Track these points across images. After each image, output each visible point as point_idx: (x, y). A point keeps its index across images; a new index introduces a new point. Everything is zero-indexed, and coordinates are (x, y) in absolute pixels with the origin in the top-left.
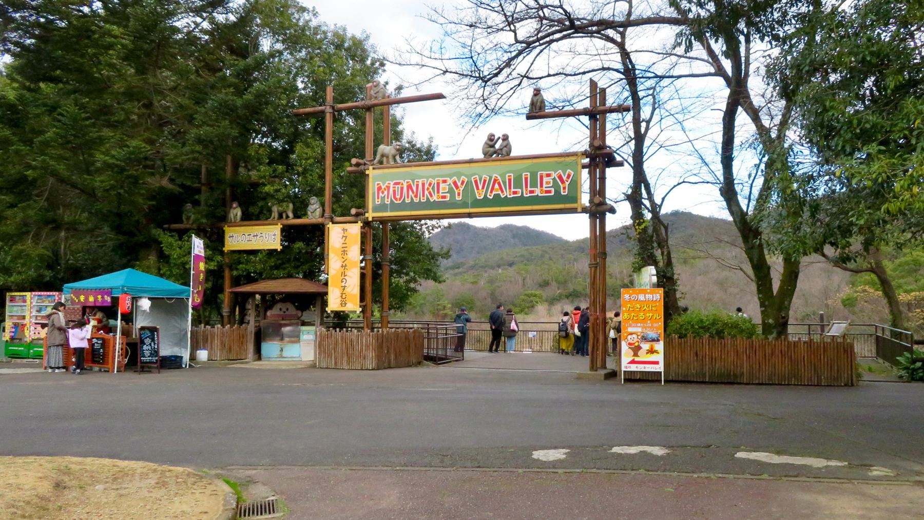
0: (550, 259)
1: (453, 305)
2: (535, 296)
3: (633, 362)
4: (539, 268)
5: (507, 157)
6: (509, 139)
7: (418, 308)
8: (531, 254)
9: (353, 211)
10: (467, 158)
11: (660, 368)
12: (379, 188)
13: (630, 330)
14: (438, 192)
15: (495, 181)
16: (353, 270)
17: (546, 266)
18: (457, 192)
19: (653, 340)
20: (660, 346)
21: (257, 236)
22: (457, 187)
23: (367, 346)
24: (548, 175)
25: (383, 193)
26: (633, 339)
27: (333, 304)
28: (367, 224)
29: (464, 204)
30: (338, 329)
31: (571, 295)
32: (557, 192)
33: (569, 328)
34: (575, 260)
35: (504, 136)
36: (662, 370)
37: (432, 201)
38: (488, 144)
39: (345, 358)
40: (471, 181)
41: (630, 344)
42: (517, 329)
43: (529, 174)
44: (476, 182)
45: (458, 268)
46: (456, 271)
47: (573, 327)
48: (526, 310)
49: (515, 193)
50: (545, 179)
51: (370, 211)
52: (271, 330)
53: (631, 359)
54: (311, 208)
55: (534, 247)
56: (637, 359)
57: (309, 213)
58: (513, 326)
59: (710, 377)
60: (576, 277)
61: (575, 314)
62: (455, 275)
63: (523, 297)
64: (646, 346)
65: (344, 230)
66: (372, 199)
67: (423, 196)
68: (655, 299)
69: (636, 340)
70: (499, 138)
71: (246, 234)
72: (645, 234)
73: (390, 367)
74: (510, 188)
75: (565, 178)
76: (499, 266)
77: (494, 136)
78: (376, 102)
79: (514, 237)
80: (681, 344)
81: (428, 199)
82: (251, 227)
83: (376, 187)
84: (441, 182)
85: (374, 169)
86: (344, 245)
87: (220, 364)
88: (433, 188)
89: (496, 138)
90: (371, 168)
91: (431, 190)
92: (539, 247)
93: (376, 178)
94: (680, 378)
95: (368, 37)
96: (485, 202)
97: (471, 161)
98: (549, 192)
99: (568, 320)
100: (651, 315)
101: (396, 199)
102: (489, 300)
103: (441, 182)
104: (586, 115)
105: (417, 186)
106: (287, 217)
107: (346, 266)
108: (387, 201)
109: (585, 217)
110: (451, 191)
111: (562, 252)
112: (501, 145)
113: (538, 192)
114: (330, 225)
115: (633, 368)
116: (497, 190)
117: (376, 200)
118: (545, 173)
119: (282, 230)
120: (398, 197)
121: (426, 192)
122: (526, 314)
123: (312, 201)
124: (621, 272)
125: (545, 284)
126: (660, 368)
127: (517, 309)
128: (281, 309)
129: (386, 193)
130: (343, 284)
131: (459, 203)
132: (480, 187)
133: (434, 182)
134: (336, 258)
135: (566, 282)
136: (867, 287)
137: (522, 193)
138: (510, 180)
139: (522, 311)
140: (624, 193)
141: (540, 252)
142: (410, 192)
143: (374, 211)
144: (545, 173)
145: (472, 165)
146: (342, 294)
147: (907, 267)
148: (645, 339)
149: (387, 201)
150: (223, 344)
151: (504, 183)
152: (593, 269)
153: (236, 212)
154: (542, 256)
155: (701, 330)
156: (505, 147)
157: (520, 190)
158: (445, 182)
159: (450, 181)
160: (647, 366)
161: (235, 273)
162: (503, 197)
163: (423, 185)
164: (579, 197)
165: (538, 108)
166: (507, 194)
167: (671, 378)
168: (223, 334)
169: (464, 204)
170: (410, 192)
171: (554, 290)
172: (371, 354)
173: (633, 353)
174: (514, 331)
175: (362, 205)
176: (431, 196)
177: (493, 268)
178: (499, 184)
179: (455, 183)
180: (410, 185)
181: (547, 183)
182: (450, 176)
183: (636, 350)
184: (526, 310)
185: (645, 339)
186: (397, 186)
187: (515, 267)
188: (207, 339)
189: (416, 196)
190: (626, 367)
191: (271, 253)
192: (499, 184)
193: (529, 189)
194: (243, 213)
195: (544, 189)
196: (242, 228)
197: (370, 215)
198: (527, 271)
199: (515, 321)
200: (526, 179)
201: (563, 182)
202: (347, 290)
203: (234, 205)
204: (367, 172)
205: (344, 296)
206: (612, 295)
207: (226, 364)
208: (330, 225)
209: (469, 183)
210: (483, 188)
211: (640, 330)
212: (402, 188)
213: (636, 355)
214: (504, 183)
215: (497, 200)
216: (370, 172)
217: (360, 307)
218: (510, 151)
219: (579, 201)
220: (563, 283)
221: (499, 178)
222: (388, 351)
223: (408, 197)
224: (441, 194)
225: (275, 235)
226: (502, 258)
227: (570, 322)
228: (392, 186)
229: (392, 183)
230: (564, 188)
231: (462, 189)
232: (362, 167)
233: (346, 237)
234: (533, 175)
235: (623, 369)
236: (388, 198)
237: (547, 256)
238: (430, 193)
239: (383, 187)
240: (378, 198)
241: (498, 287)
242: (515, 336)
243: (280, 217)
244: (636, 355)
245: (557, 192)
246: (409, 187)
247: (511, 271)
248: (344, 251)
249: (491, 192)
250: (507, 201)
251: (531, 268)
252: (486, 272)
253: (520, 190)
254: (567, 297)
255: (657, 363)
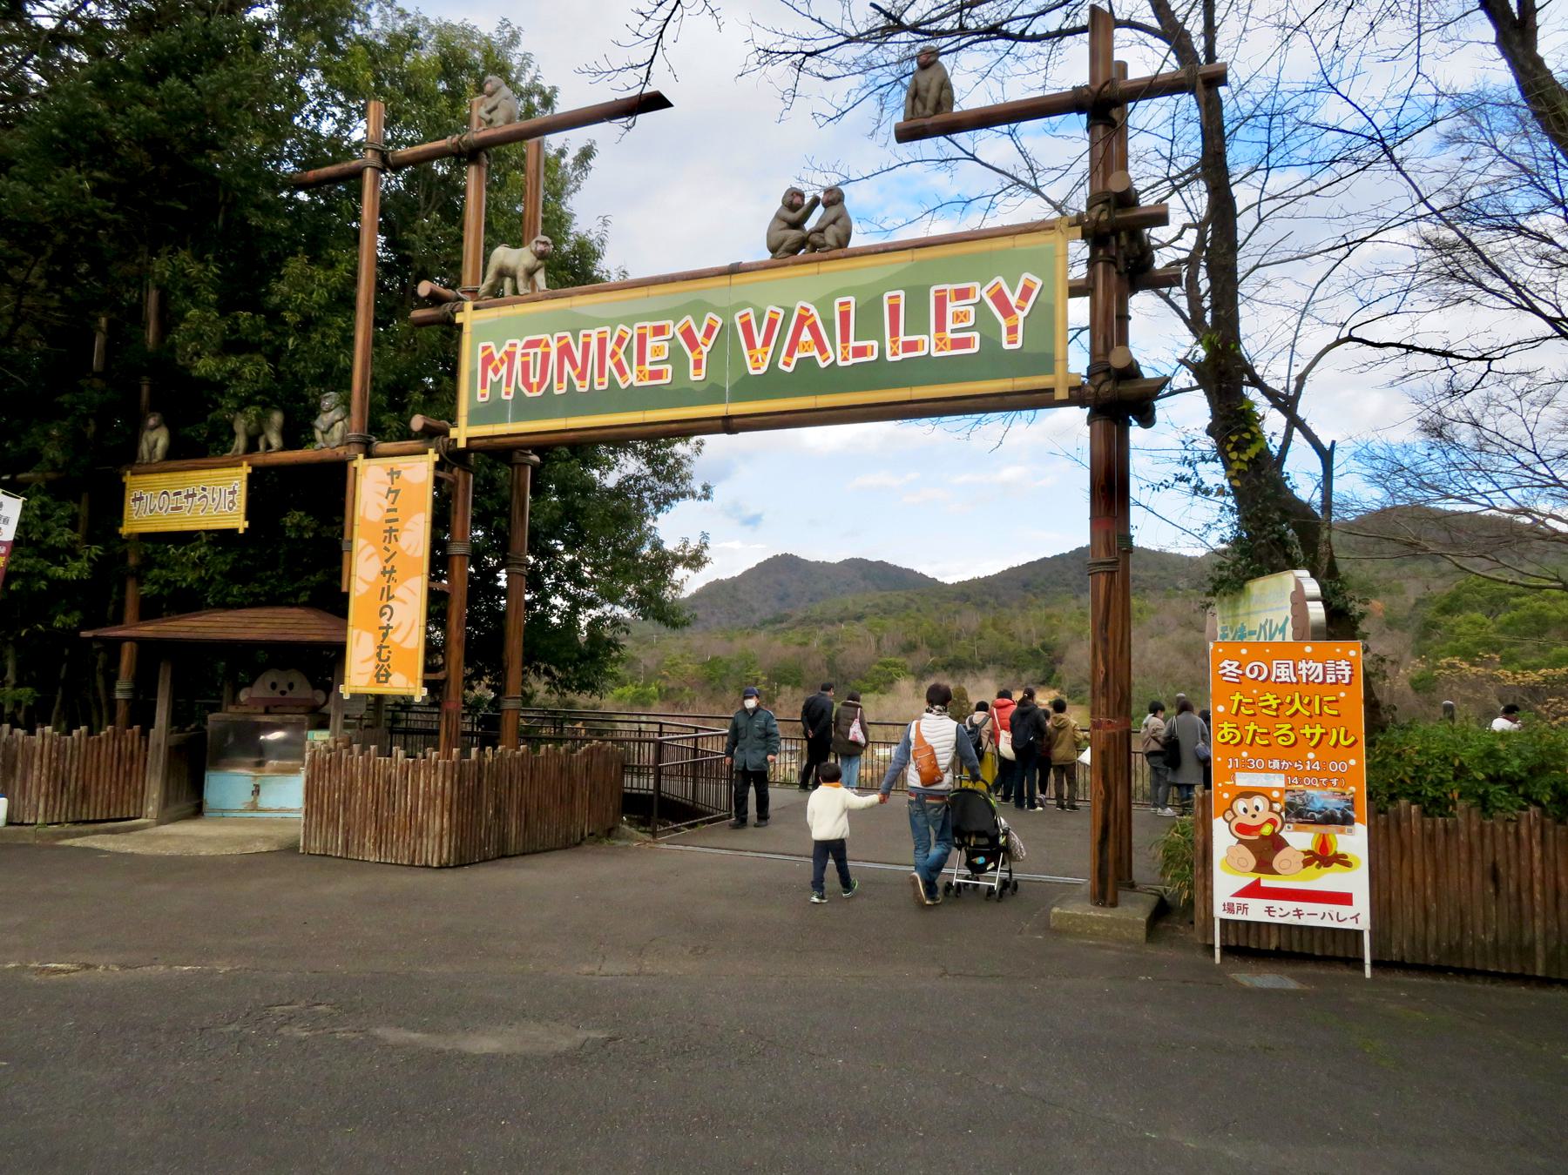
0: (918, 610)
1: (769, 676)
2: (895, 665)
3: (1254, 891)
4: (901, 623)
5: (839, 252)
6: (846, 203)
7: (717, 681)
8: (890, 603)
9: (417, 422)
10: (724, 262)
11: (1358, 916)
12: (488, 359)
13: (1243, 780)
14: (641, 361)
15: (802, 320)
16: (409, 583)
17: (912, 621)
18: (691, 357)
19: (1329, 819)
20: (1354, 841)
21: (194, 495)
22: (693, 344)
23: (429, 799)
24: (962, 294)
25: (496, 371)
26: (1257, 812)
27: (358, 677)
28: (452, 459)
29: (713, 393)
30: (356, 747)
31: (950, 665)
32: (990, 342)
33: (985, 740)
34: (957, 612)
35: (828, 191)
36: (1364, 924)
37: (623, 386)
38: (784, 220)
39: (370, 832)
40: (734, 326)
41: (1242, 828)
42: (862, 740)
43: (902, 293)
44: (747, 326)
45: (781, 622)
46: (778, 626)
47: (994, 736)
48: (882, 686)
49: (860, 352)
50: (952, 307)
51: (463, 419)
52: (231, 739)
53: (1247, 879)
54: (322, 422)
55: (896, 593)
56: (1268, 882)
57: (318, 435)
58: (855, 732)
59: (1552, 958)
60: (958, 638)
61: (999, 707)
62: (775, 633)
63: (876, 667)
64: (1300, 840)
65: (394, 474)
66: (471, 391)
67: (601, 374)
68: (1331, 679)
69: (1264, 814)
70: (815, 202)
71: (171, 492)
72: (1258, 474)
73: (503, 855)
74: (845, 339)
75: (1013, 300)
76: (841, 621)
77: (802, 195)
78: (490, 133)
79: (864, 578)
80: (1432, 838)
81: (612, 381)
82: (181, 475)
83: (480, 355)
84: (649, 332)
85: (476, 308)
86: (392, 515)
87: (37, 836)
88: (628, 352)
89: (807, 201)
90: (469, 305)
91: (621, 355)
92: (902, 593)
93: (482, 332)
94: (1432, 958)
95: (514, 39)
96: (772, 382)
97: (734, 270)
98: (966, 343)
99: (985, 722)
100: (1318, 731)
101: (529, 387)
102: (825, 671)
103: (649, 332)
104: (1080, 110)
105: (586, 346)
106: (269, 446)
107: (393, 570)
108: (507, 395)
109: (1077, 416)
110: (676, 357)
111: (936, 600)
112: (820, 220)
113: (928, 345)
114: (360, 462)
115: (1256, 911)
116: (806, 347)
117: (479, 391)
118: (950, 288)
119: (251, 479)
120: (534, 380)
121: (609, 363)
122: (882, 693)
123: (326, 403)
124: (1028, 631)
125: (910, 648)
126: (1358, 916)
127: (868, 686)
128: (274, 686)
129: (504, 370)
130: (384, 621)
131: (698, 388)
132: (759, 341)
133: (632, 332)
134: (370, 549)
135: (943, 644)
136: (1456, 660)
137: (882, 351)
138: (845, 316)
139: (875, 688)
140: (1183, 362)
141: (903, 601)
142: (567, 366)
143: (470, 423)
144: (950, 288)
145: (737, 279)
146: (380, 647)
147: (1523, 627)
148: (1298, 813)
149: (507, 395)
150: (58, 781)
151: (829, 325)
152: (1103, 580)
153: (157, 439)
154: (906, 607)
155: (1492, 788)
156: (834, 222)
157: (875, 343)
158: (659, 331)
159: (674, 329)
160: (1306, 907)
161: (146, 589)
162: (823, 365)
163: (602, 342)
164: (1059, 355)
165: (931, 103)
166: (837, 355)
167: (1395, 954)
168: (61, 752)
169: (713, 393)
170: (567, 366)
171: (924, 657)
172: (437, 823)
173: (1253, 862)
174: (855, 744)
175: (443, 402)
176: (622, 372)
177: (832, 623)
178: (814, 330)
179: (688, 334)
180: (568, 345)
181: (958, 317)
182: (676, 315)
183: (1266, 849)
184: (882, 686)
185: (1299, 814)
186: (532, 351)
187: (865, 622)
188: (14, 767)
189: (581, 377)
190: (1229, 908)
191: (224, 537)
192: (814, 330)
193: (902, 338)
194: (173, 438)
195: (949, 335)
196: (164, 476)
197: (461, 433)
198: (883, 628)
199: (862, 722)
200: (894, 309)
201: (1007, 310)
202: (395, 637)
203: (152, 422)
204: (459, 318)
205: (384, 655)
206: (1015, 666)
207: (59, 836)
208: (360, 462)
209: (727, 329)
210: (766, 343)
211: (1278, 781)
212: (546, 356)
213: (1264, 866)
214: (829, 325)
215: (809, 376)
216: (467, 317)
217: (426, 683)
218: (848, 236)
219: (1059, 367)
220: (937, 647)
221: (813, 310)
222: (497, 811)
223: (560, 380)
224: (648, 367)
225: (233, 492)
226: (846, 609)
227: (988, 727)
228: (519, 351)
229: (520, 344)
230: (1012, 330)
231: (706, 350)
232: (447, 307)
233: (397, 492)
234: (917, 297)
235: (1219, 913)
236: (508, 385)
237: (914, 606)
238: (619, 365)
239: (497, 356)
240: (484, 386)
241: (841, 651)
242: (859, 754)
243: (252, 447)
244: (1264, 866)
245: (990, 342)
246: (565, 351)
247: (858, 628)
248: (391, 530)
249: (790, 354)
250: (836, 378)
251: (890, 622)
252: (822, 628)
253: (875, 343)
254: (945, 668)
255: (1345, 899)
